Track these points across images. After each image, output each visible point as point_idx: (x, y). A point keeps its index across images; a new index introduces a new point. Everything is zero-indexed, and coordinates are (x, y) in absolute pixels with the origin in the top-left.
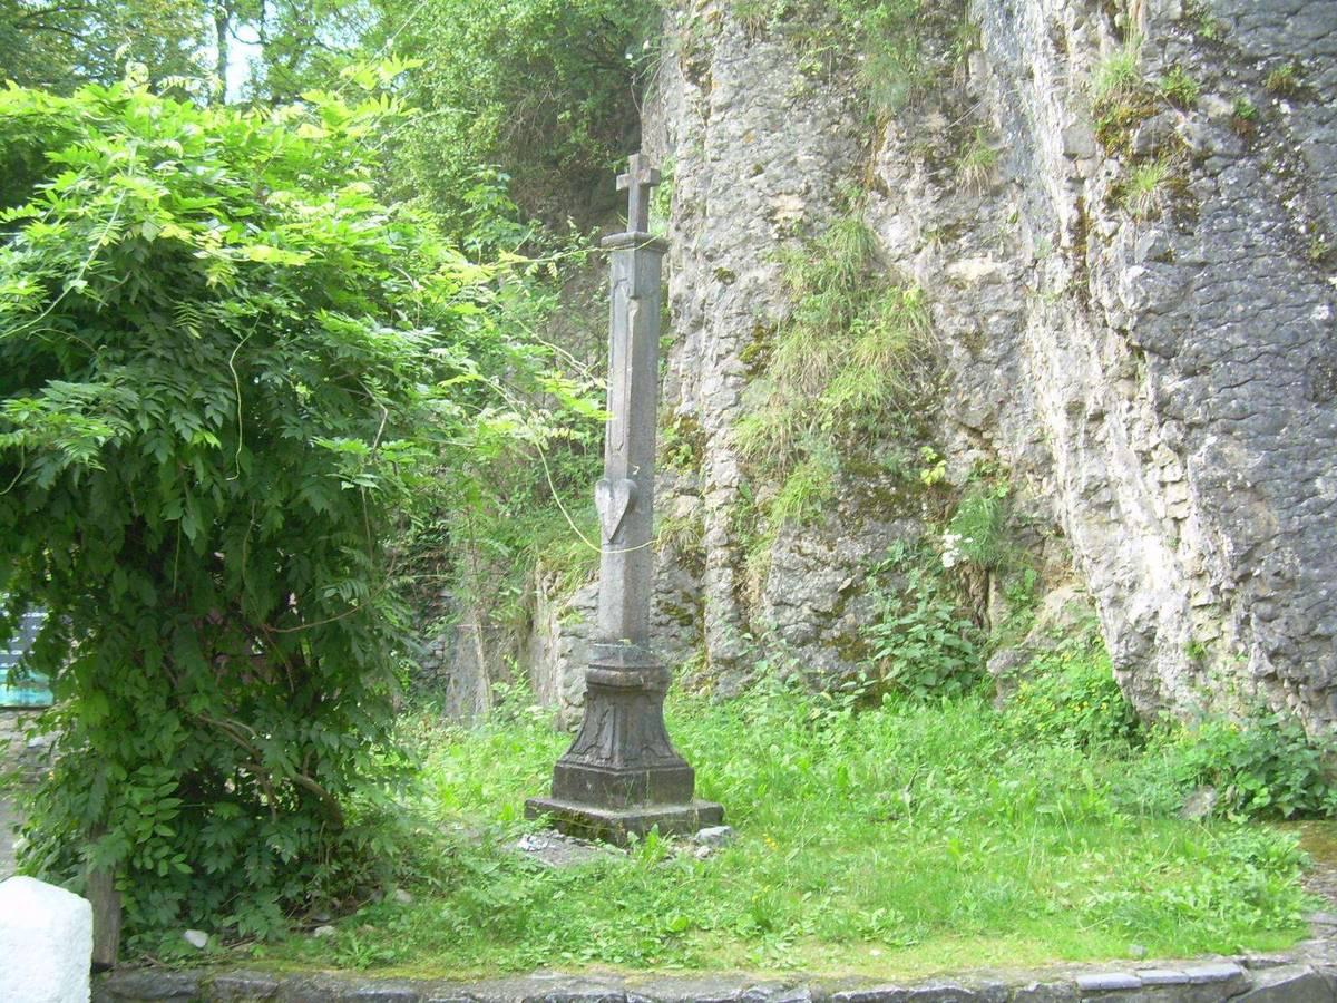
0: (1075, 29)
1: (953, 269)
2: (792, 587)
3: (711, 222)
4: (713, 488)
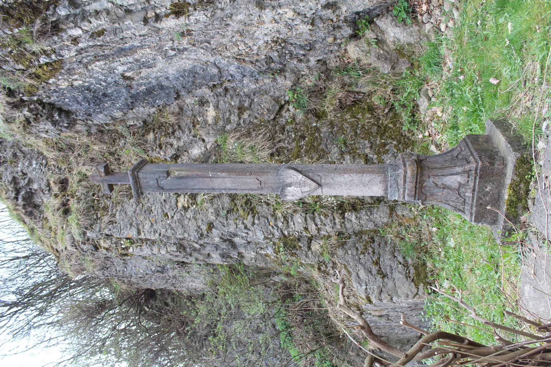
0: (91, 23)
1: (210, 122)
3: (186, 235)
4: (306, 229)
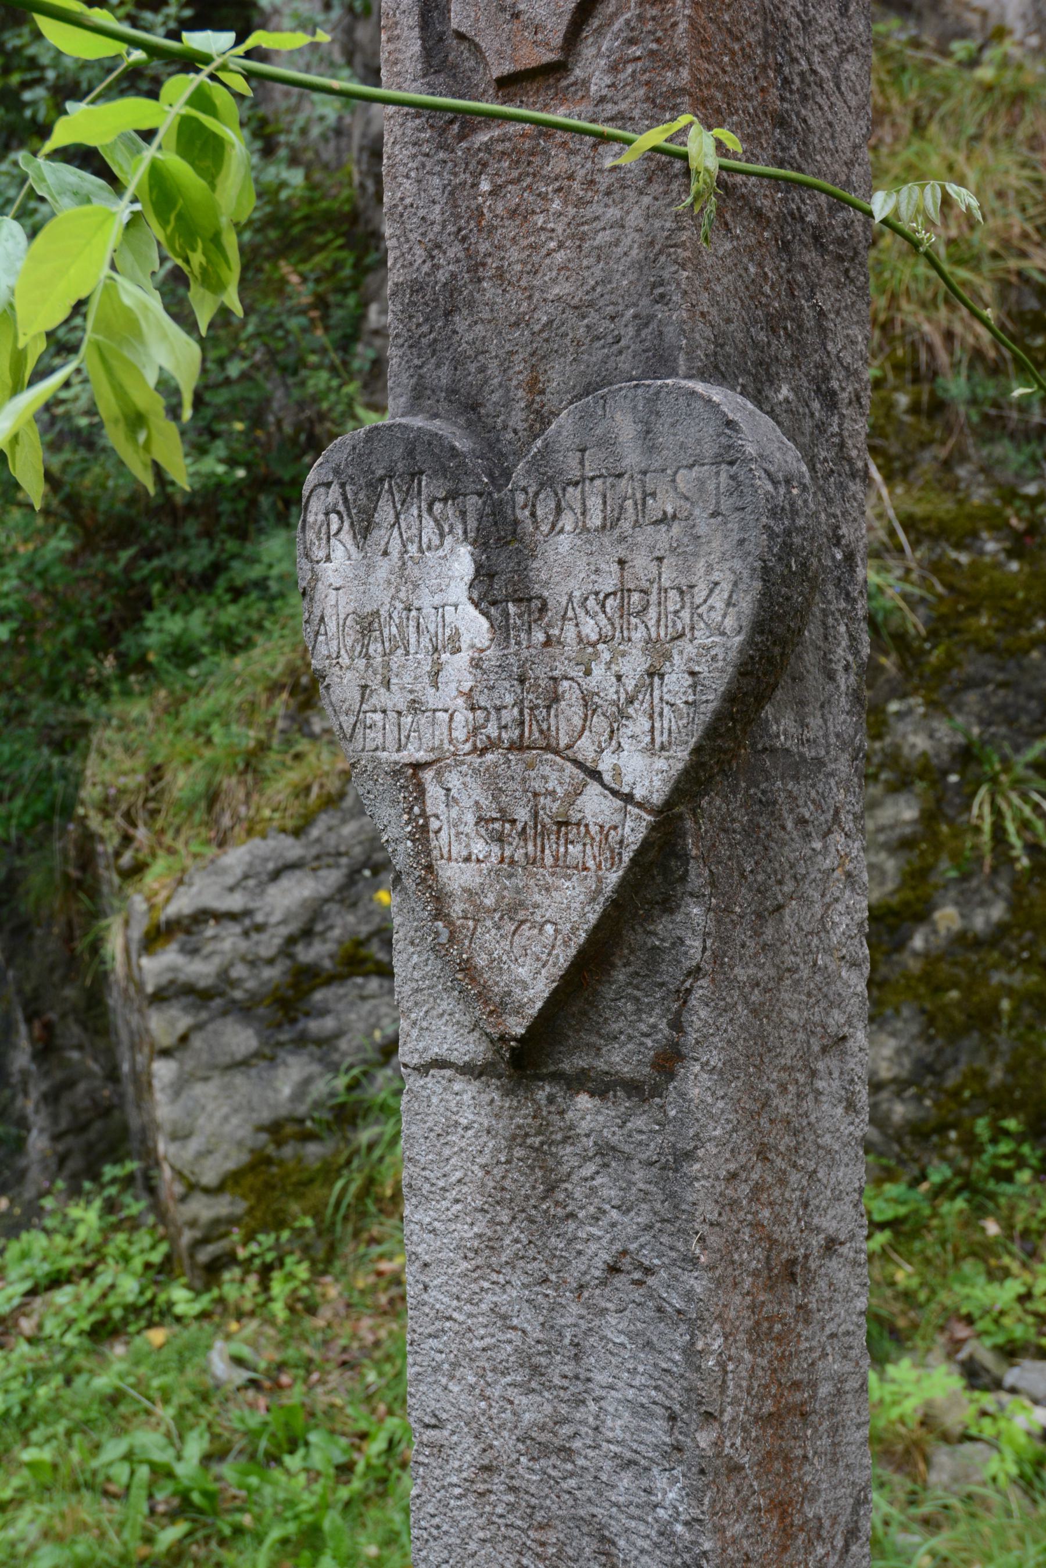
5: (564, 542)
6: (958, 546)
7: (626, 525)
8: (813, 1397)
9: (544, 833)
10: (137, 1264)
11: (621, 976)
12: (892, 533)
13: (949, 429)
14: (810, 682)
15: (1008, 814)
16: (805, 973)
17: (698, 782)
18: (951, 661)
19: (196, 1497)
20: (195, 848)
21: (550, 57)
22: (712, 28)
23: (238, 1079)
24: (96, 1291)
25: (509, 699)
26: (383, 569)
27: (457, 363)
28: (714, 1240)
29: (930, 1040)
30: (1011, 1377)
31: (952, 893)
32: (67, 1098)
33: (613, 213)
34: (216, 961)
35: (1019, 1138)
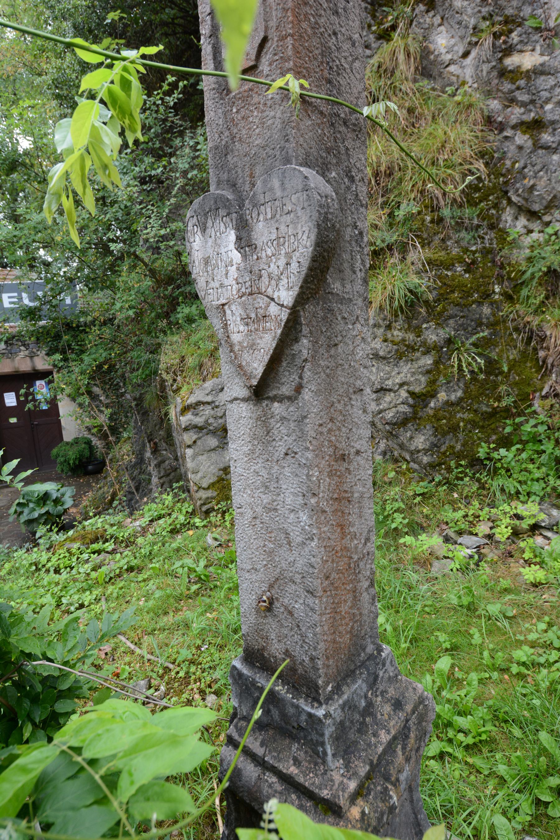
2: (389, 373)
5: (261, 224)
6: (447, 269)
7: (278, 216)
8: (352, 496)
9: (259, 321)
10: (184, 512)
11: (284, 364)
12: (424, 266)
13: (444, 228)
14: (346, 273)
15: (463, 361)
16: (347, 367)
17: (303, 298)
18: (444, 309)
19: (202, 577)
20: (195, 382)
21: (252, 63)
22: (301, 48)
23: (213, 454)
24: (171, 520)
25: (248, 279)
26: (210, 242)
27: (229, 171)
28: (314, 442)
29: (436, 436)
30: (460, 540)
31: (444, 388)
32: (163, 466)
33: (272, 113)
34: (204, 417)
35: (466, 467)
